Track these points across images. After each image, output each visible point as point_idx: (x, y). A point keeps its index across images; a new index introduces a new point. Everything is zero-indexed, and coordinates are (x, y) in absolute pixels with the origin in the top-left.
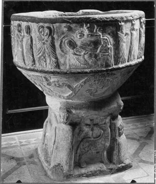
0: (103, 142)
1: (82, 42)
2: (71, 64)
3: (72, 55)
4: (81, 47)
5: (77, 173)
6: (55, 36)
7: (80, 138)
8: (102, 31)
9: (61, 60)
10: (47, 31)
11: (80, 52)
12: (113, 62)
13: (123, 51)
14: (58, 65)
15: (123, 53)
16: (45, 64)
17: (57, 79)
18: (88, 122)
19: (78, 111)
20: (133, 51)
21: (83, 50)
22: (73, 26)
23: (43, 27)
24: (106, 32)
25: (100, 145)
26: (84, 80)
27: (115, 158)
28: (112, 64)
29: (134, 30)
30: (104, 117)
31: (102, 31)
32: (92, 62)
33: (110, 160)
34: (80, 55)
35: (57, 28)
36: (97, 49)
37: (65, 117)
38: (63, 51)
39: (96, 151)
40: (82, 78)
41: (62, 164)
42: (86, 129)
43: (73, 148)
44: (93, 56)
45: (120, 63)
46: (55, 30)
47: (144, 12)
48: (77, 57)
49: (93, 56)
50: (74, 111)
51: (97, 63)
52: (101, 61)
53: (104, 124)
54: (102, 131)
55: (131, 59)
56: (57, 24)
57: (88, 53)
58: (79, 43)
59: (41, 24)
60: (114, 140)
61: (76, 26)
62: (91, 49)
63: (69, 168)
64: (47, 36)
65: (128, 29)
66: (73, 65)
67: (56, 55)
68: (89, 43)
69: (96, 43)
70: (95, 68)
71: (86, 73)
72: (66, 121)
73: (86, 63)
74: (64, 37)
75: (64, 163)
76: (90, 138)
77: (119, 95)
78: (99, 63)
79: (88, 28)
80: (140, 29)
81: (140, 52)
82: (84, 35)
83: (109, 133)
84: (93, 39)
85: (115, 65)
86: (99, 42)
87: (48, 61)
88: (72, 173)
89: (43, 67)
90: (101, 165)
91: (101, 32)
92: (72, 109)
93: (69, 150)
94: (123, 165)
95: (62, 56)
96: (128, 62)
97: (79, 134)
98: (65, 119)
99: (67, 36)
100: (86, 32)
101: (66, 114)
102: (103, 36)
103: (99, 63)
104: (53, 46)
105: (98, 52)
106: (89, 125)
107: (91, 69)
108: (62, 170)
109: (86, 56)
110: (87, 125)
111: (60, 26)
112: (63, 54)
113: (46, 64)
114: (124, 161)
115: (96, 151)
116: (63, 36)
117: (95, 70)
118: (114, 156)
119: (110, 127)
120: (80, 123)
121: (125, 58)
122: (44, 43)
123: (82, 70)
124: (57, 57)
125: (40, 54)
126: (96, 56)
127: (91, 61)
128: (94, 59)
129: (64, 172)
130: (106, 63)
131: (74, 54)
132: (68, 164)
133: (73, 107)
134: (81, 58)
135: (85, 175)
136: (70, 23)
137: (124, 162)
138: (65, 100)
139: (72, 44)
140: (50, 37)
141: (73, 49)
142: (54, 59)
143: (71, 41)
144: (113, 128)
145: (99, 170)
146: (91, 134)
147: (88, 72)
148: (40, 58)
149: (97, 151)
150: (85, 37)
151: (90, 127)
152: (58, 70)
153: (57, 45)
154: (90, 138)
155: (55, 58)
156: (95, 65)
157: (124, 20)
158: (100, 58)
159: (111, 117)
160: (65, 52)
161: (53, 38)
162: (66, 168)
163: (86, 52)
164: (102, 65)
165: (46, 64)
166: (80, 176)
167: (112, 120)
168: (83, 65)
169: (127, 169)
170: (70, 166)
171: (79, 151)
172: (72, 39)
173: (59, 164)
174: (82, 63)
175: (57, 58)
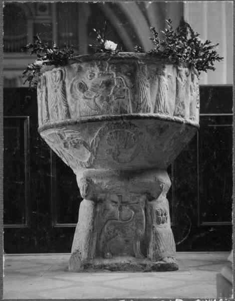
0: (134, 227)
3: (82, 99)
4: (92, 90)
5: (98, 264)
6: (67, 81)
7: (104, 218)
9: (72, 108)
11: (91, 95)
12: (131, 108)
13: (144, 97)
14: (68, 115)
15: (144, 99)
17: (69, 134)
18: (115, 198)
19: (100, 181)
20: (163, 100)
24: (120, 72)
25: (130, 231)
26: (98, 132)
27: (151, 252)
28: (129, 111)
30: (136, 195)
32: (104, 106)
33: (144, 252)
34: (90, 99)
36: (110, 91)
38: (73, 96)
39: (124, 239)
42: (112, 207)
43: (93, 230)
44: (105, 99)
45: (141, 111)
48: (87, 101)
49: (105, 99)
50: (95, 181)
51: (109, 107)
52: (114, 105)
53: (137, 203)
54: (133, 212)
55: (160, 110)
57: (99, 96)
58: (89, 85)
60: (149, 227)
62: (103, 92)
63: (88, 255)
66: (83, 111)
67: (67, 102)
70: (108, 114)
71: (97, 120)
72: (86, 192)
73: (97, 108)
76: (117, 220)
78: (112, 107)
79: (98, 66)
80: (177, 78)
82: (94, 74)
83: (143, 216)
84: (105, 79)
85: (134, 112)
86: (112, 82)
87: (59, 110)
90: (131, 259)
91: (115, 70)
92: (93, 177)
93: (88, 231)
94: (162, 262)
96: (155, 112)
97: (103, 213)
100: (97, 71)
101: (85, 183)
102: (117, 76)
103: (112, 107)
105: (111, 94)
106: (116, 203)
107: (103, 116)
109: (97, 100)
110: (113, 202)
114: (164, 258)
115: (124, 239)
116: (73, 79)
117: (107, 117)
118: (150, 249)
119: (145, 209)
120: (105, 200)
121: (149, 106)
126: (108, 99)
127: (103, 105)
128: (105, 102)
130: (121, 108)
133: (94, 176)
134: (92, 102)
135: (108, 268)
137: (164, 259)
138: (87, 170)
139: (83, 87)
141: (83, 93)
142: (64, 108)
143: (81, 83)
144: (149, 211)
145: (127, 263)
146: (119, 215)
147: (100, 119)
149: (126, 239)
150: (96, 76)
151: (117, 205)
152: (69, 120)
153: (68, 89)
154: (117, 220)
156: (107, 110)
158: (112, 102)
159: (147, 196)
160: (75, 97)
161: (64, 83)
162: (84, 255)
164: (116, 111)
166: (102, 268)
167: (148, 200)
169: (169, 269)
170: (89, 254)
171: (103, 237)
172: (83, 81)
173: (78, 251)
174: (93, 108)
175: (67, 106)
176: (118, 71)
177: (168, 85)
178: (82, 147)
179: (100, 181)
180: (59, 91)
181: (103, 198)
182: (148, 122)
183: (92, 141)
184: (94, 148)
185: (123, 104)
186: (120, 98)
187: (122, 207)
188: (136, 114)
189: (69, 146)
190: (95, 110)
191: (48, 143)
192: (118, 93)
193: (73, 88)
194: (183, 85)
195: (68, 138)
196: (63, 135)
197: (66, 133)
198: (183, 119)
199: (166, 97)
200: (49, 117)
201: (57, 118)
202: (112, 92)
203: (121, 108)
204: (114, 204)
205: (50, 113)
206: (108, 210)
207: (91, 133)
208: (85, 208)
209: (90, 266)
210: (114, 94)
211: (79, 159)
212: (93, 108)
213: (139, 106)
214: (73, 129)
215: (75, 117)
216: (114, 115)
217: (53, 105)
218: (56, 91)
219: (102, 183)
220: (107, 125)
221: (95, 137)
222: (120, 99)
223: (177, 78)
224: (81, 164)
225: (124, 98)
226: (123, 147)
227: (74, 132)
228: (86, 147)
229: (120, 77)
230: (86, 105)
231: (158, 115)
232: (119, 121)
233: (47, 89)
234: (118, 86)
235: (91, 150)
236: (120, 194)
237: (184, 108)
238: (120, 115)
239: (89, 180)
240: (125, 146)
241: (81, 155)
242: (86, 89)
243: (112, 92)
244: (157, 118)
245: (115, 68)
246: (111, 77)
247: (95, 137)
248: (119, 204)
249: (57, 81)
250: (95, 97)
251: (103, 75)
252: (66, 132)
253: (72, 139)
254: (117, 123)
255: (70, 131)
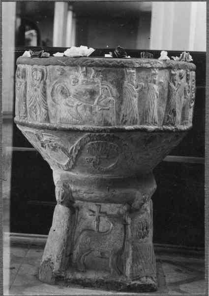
1: (76, 90)
2: (62, 117)
3: (64, 106)
4: (75, 96)
6: (48, 81)
8: (101, 77)
9: (52, 112)
10: (40, 75)
14: (48, 119)
16: (35, 116)
17: (48, 137)
21: (76, 100)
22: (67, 68)
23: (36, 70)
24: (106, 80)
29: (155, 83)
31: (101, 77)
34: (72, 106)
35: (50, 71)
36: (94, 100)
37: (60, 193)
38: (54, 100)
40: (77, 138)
41: (53, 260)
46: (48, 74)
47: (195, 64)
48: (69, 108)
54: (112, 225)
55: (147, 121)
56: (51, 67)
58: (72, 90)
59: (35, 66)
61: (70, 70)
64: (39, 81)
65: (142, 80)
67: (47, 104)
68: (84, 92)
69: (93, 93)
71: (78, 131)
72: (62, 199)
74: (57, 82)
75: (54, 258)
77: (155, 182)
80: (169, 83)
81: (168, 116)
84: (89, 87)
87: (38, 113)
88: (63, 275)
89: (34, 120)
95: (53, 106)
98: (60, 197)
99: (60, 82)
100: (81, 78)
101: (62, 189)
102: (102, 85)
104: (44, 92)
105: (95, 104)
106: (93, 212)
108: (52, 268)
109: (80, 108)
111: (53, 69)
112: (54, 104)
113: (36, 116)
116: (55, 82)
122: (36, 89)
123: (74, 126)
124: (47, 108)
125: (32, 103)
126: (91, 109)
129: (54, 271)
131: (65, 105)
132: (59, 260)
134: (73, 110)
136: (64, 65)
138: (65, 172)
139: (65, 93)
140: (42, 82)
142: (44, 110)
147: (81, 129)
148: (30, 108)
151: (95, 215)
152: (48, 124)
153: (49, 92)
155: (45, 109)
157: (135, 66)
158: (96, 113)
161: (45, 84)
162: (56, 266)
163: (80, 104)
165: (36, 116)
168: (75, 120)
173: (50, 259)
175: (47, 109)
176: (105, 78)
177: (158, 94)
178: (60, 152)
179: (78, 188)
180: (40, 91)
181: (80, 205)
182: (135, 136)
183: (71, 148)
184: (74, 155)
185: (107, 115)
186: (104, 110)
187: (101, 217)
188: (121, 127)
189: (47, 147)
190: (77, 119)
191: (28, 138)
192: (102, 103)
193: (55, 91)
194: (176, 89)
195: (46, 140)
196: (41, 136)
197: (43, 136)
198: (173, 128)
199: (156, 106)
200: (27, 114)
201: (35, 119)
202: (96, 101)
203: (105, 121)
204: (91, 213)
205: (28, 110)
206: (85, 219)
207: (71, 141)
208: (60, 213)
209: (62, 279)
210: (97, 104)
211: (56, 161)
212: (74, 116)
213: (125, 117)
214: (53, 134)
215: (54, 123)
216: (97, 127)
217: (32, 103)
218: (36, 90)
219: (79, 191)
220: (89, 136)
221: (75, 145)
222: (104, 111)
223: (169, 83)
224: (59, 166)
225: (109, 110)
226: (106, 157)
227: (53, 136)
228: (64, 152)
229: (106, 87)
230: (67, 112)
231: (145, 126)
232: (102, 134)
233: (26, 83)
234: (103, 96)
235: (70, 155)
236: (99, 204)
237: (175, 115)
238: (103, 128)
239: (65, 186)
240: (108, 156)
241: (59, 157)
242: (68, 95)
243: (96, 101)
244: (145, 130)
245: (101, 76)
246: (96, 85)
247: (75, 145)
248: (97, 214)
249: (38, 80)
250: (78, 105)
251: (87, 83)
252: (45, 135)
253: (50, 142)
254: (99, 135)
255: (49, 134)
